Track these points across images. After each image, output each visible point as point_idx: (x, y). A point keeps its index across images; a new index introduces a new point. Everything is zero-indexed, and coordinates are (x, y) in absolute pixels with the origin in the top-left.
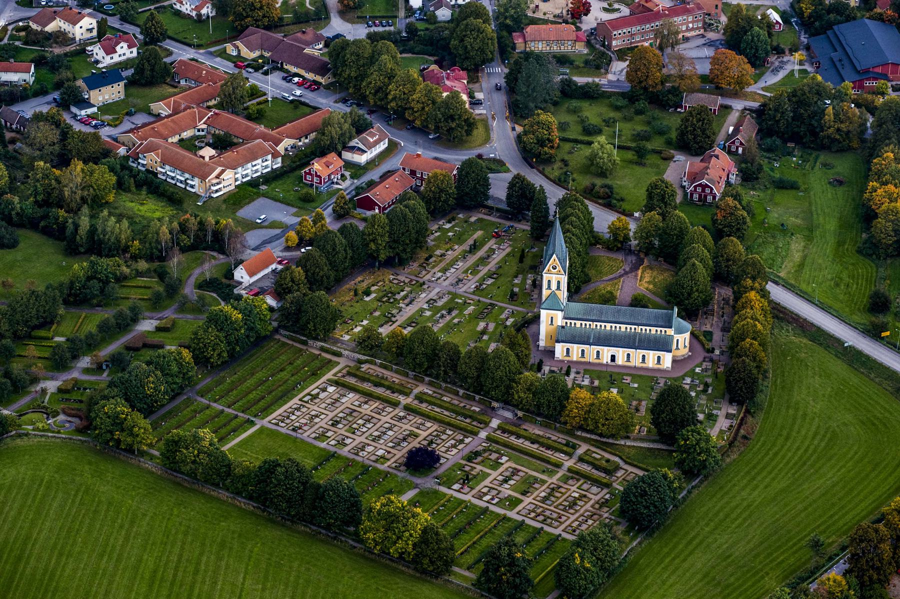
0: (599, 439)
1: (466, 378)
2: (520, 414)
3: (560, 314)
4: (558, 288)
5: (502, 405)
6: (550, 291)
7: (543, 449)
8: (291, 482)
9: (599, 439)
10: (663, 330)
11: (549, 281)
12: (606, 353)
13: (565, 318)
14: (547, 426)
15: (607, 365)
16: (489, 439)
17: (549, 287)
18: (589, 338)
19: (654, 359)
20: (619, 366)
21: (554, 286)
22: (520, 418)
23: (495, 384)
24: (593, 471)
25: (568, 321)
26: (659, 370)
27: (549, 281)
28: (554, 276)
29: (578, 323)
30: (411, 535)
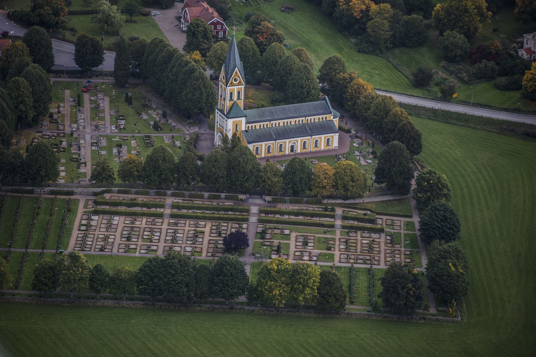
0: (343, 202)
1: (216, 179)
2: (268, 198)
3: (243, 120)
4: (239, 98)
5: (248, 195)
6: (232, 102)
7: (309, 218)
8: (186, 268)
9: (343, 202)
10: (324, 116)
11: (231, 93)
12: (287, 143)
13: (247, 123)
14: (267, 211)
15: (289, 155)
16: (260, 221)
17: (231, 99)
18: (271, 136)
19: (325, 141)
20: (299, 154)
21: (235, 98)
22: (269, 202)
23: (246, 177)
24: (360, 223)
25: (250, 125)
26: (329, 151)
27: (231, 93)
28: (236, 87)
29: (258, 125)
30: (314, 282)
